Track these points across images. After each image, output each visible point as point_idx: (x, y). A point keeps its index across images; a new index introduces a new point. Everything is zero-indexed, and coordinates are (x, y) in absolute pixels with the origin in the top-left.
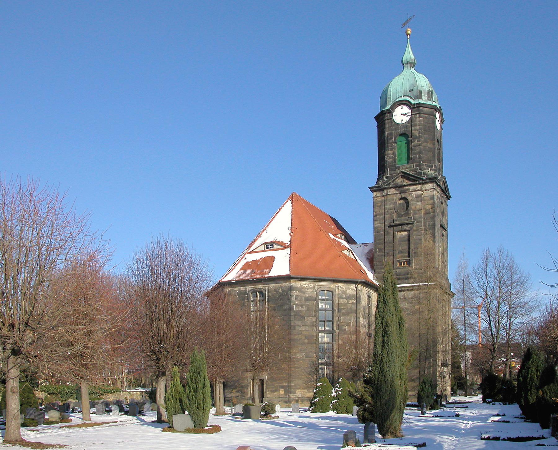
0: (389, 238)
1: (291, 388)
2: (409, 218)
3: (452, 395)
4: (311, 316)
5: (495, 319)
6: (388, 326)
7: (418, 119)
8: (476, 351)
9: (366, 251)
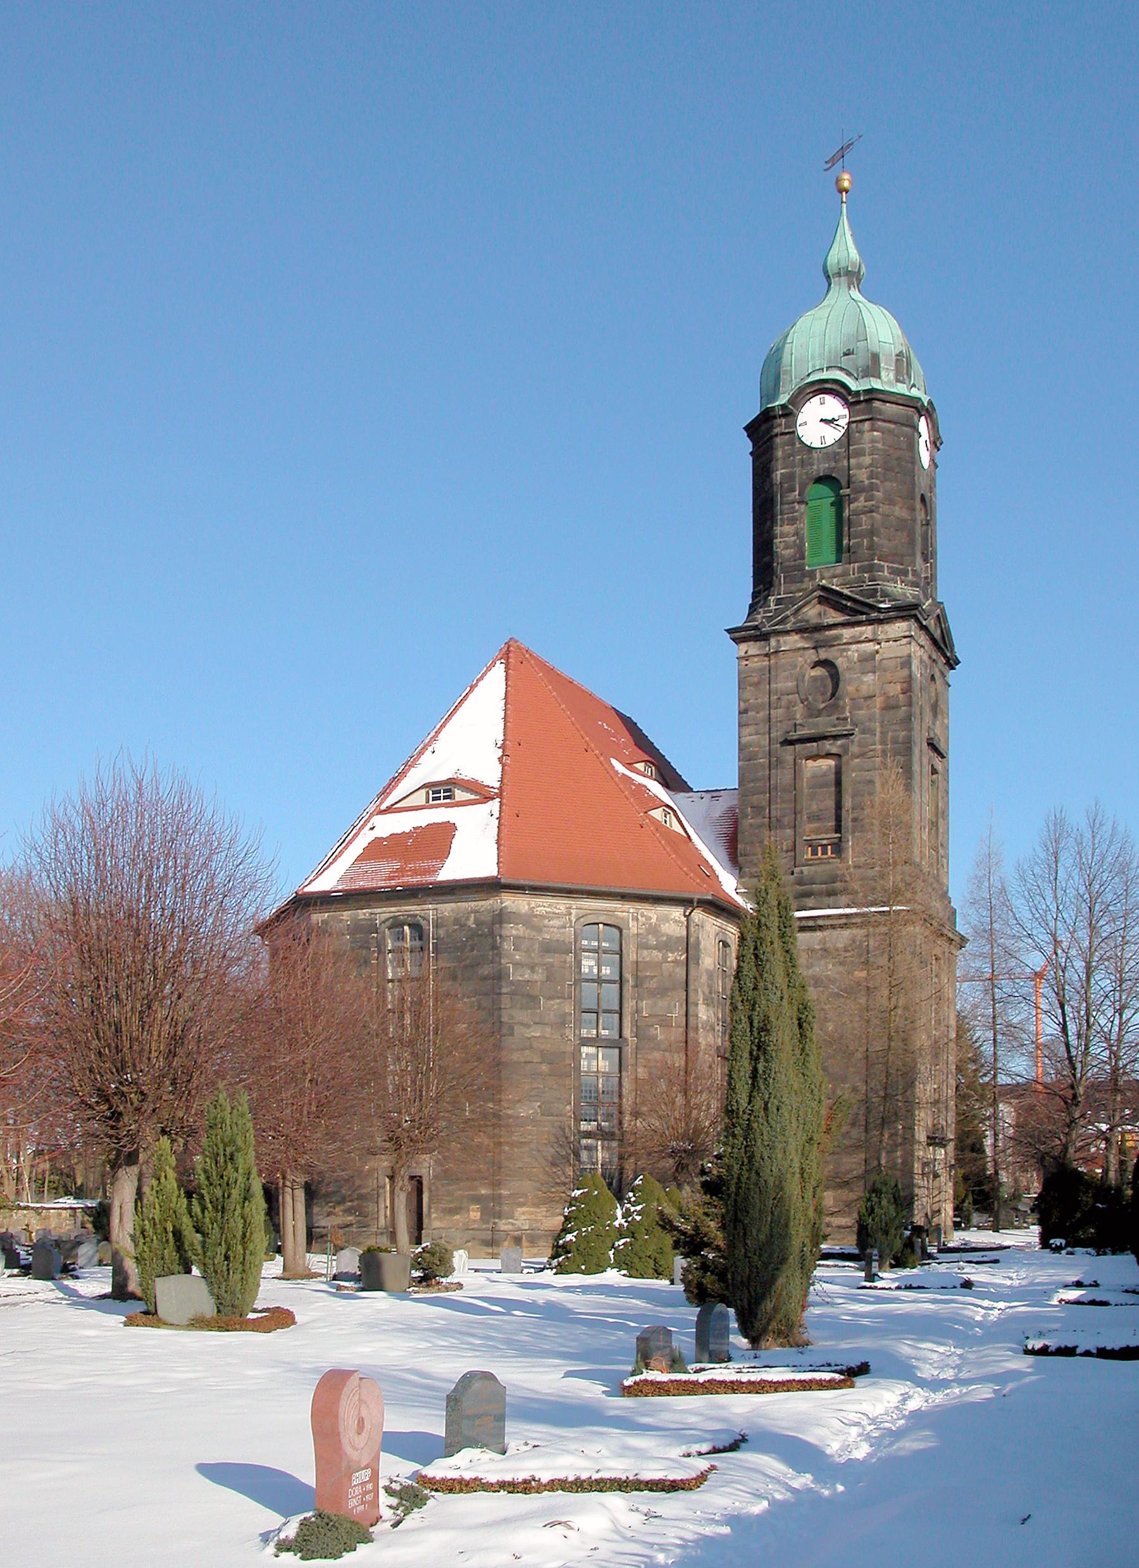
0: (784, 777)
1: (500, 1204)
2: (838, 719)
3: (957, 1226)
4: (559, 998)
5: (1078, 1012)
6: (768, 1031)
7: (867, 436)
8: (1027, 1101)
9: (717, 814)
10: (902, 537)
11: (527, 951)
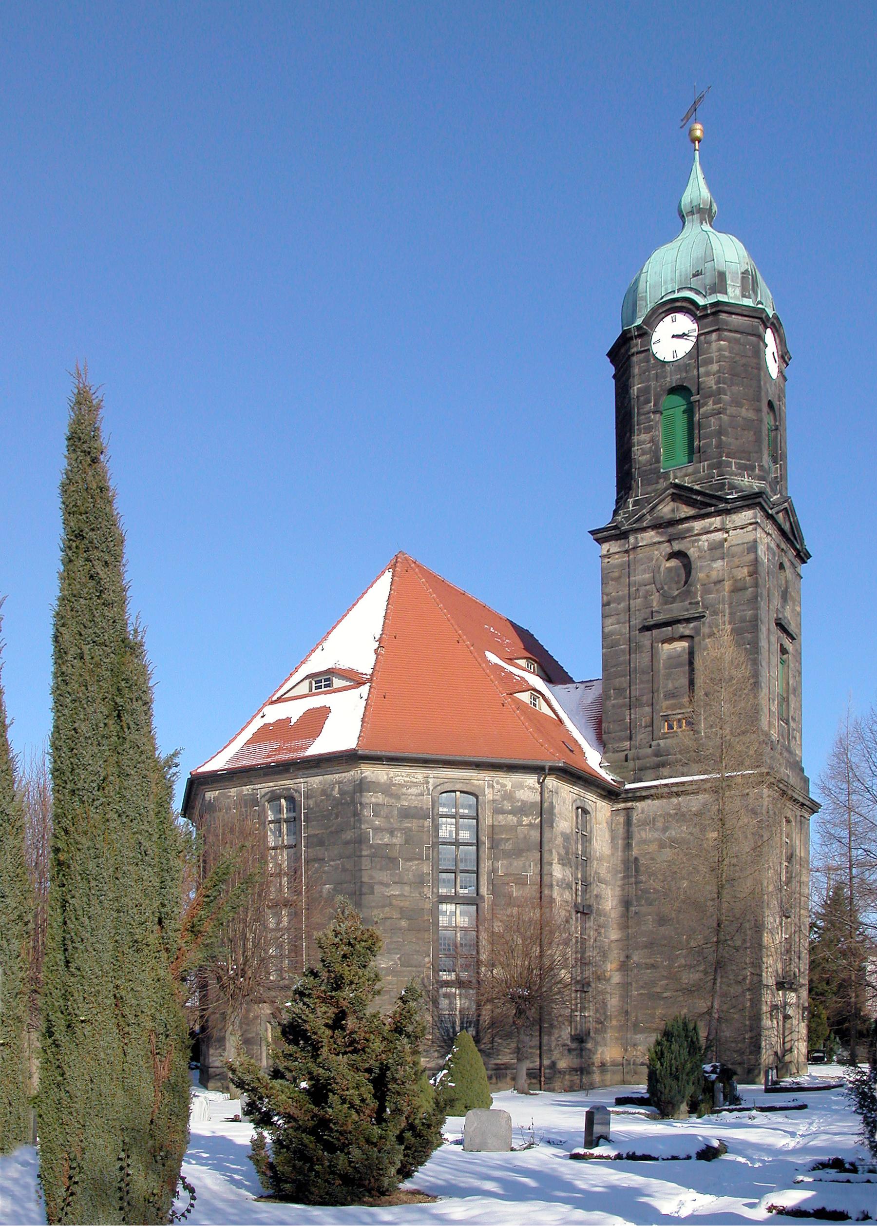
0: (642, 659)
2: (690, 603)
4: (419, 859)
7: (714, 346)
10: (750, 435)
11: (387, 817)
